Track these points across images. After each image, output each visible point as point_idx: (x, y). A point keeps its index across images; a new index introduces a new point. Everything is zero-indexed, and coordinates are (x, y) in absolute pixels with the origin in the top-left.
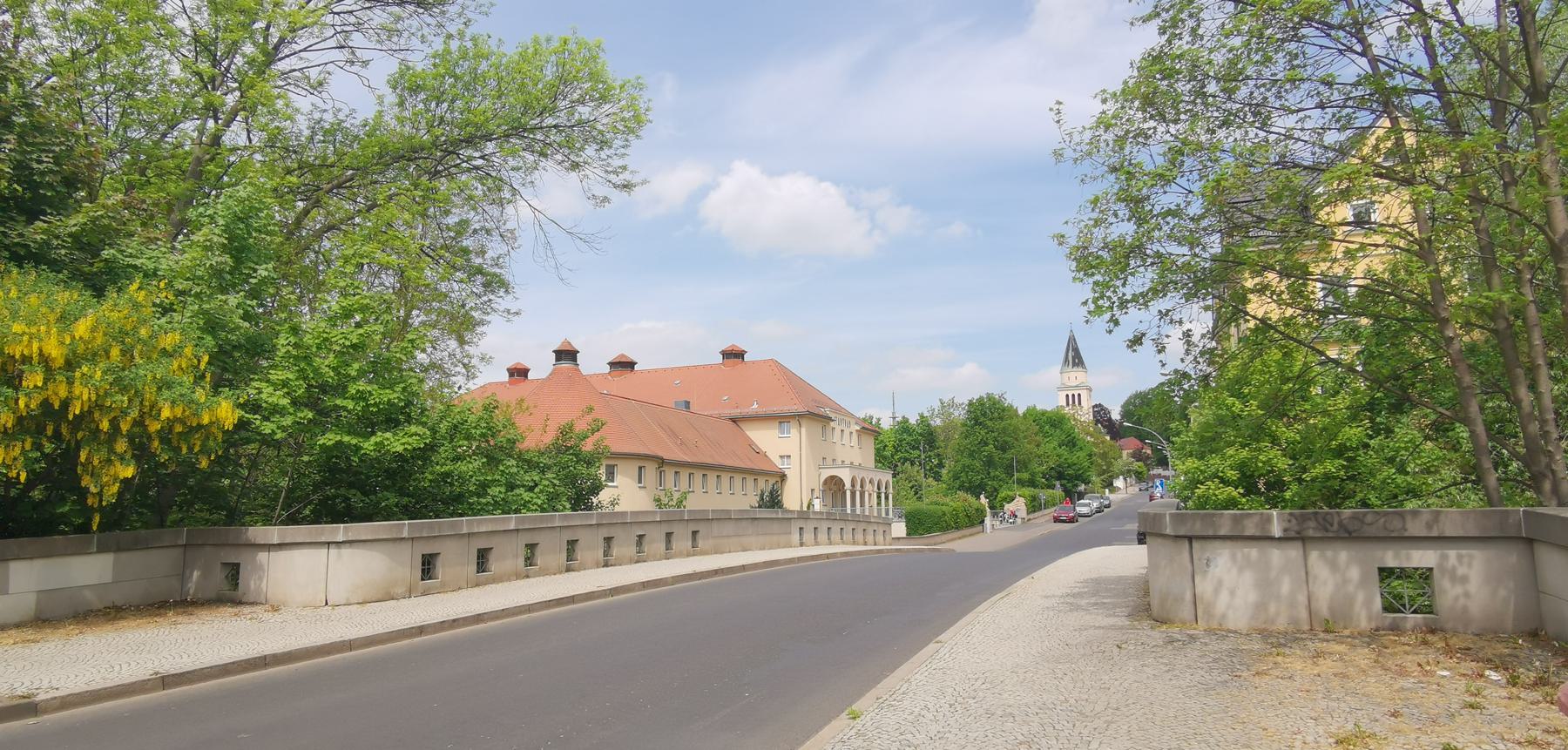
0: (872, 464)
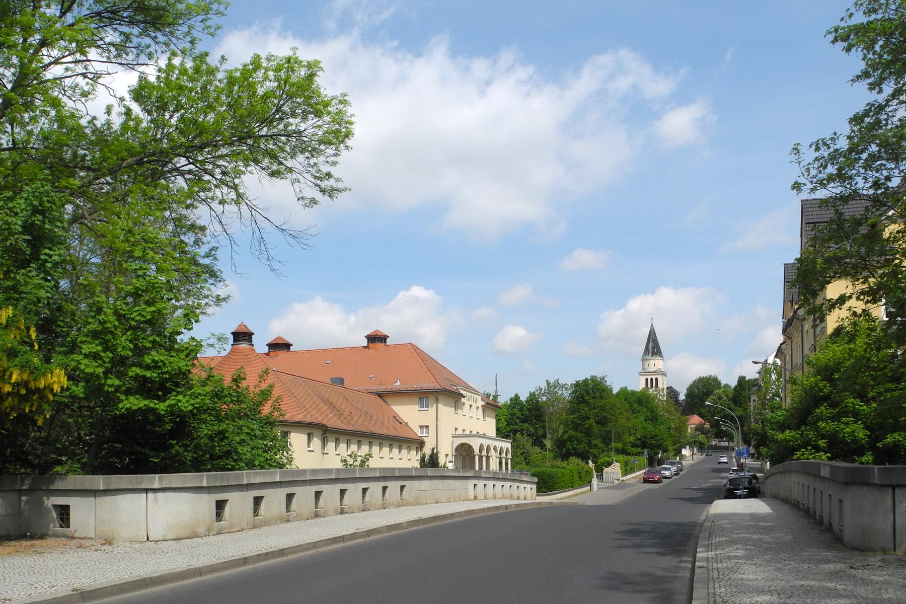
0: (494, 435)
